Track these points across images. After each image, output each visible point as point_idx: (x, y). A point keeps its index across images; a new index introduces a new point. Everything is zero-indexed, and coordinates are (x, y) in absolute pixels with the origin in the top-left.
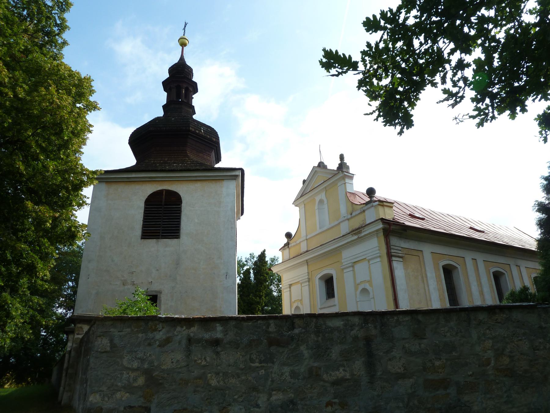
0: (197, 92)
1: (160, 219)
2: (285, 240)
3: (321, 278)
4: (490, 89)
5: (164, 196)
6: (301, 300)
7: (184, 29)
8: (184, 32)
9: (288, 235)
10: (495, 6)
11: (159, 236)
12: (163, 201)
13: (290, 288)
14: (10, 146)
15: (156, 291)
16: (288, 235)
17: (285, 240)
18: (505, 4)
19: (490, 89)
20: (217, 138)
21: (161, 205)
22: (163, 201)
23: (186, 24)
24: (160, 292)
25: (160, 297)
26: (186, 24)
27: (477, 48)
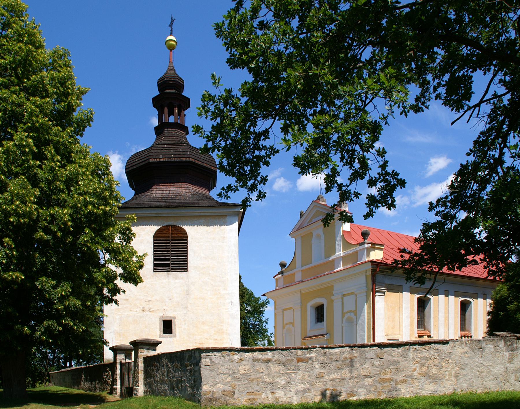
0: (189, 99)
1: (169, 254)
2: (279, 269)
3: (311, 306)
4: (474, 213)
5: (170, 232)
6: (293, 324)
7: (171, 26)
8: (171, 30)
9: (283, 265)
10: (496, 125)
11: (168, 265)
12: (170, 237)
13: (283, 312)
14: (61, 294)
15: (170, 317)
16: (283, 265)
17: (279, 269)
18: (487, 258)
19: (474, 213)
20: (213, 162)
21: (169, 240)
22: (170, 237)
23: (173, 21)
24: (175, 318)
25: (175, 322)
26: (173, 21)
27: (472, 149)
